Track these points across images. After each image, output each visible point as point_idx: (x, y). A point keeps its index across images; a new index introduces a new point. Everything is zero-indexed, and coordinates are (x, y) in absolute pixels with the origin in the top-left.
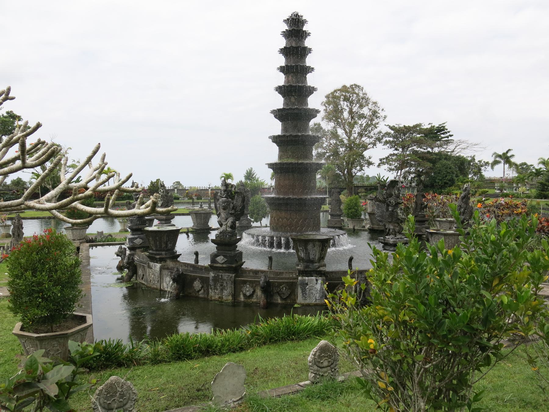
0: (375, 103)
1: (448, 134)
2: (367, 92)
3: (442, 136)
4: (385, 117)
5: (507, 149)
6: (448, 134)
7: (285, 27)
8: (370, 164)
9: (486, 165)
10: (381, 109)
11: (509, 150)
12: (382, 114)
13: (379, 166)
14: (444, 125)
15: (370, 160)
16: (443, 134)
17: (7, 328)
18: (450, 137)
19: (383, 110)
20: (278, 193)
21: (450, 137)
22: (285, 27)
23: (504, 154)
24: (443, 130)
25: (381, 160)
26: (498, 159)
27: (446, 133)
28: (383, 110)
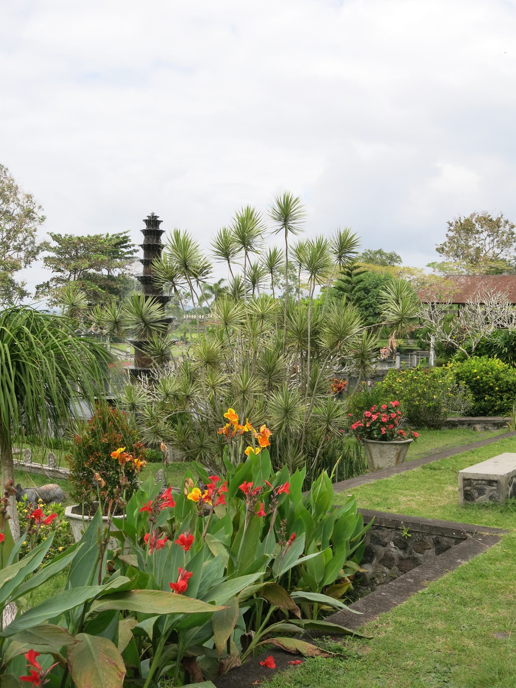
0: (29, 197)
1: (132, 249)
2: (14, 177)
3: (124, 250)
4: (43, 219)
5: (220, 279)
6: (132, 249)
7: (144, 227)
8: (23, 294)
9: (186, 298)
10: (37, 205)
11: (222, 280)
12: (39, 213)
13: (37, 297)
14: (127, 235)
15: (25, 288)
16: (125, 247)
17: (460, 375)
18: (134, 253)
19: (40, 207)
20: (136, 366)
21: (134, 253)
22: (144, 227)
23: (216, 285)
24: (126, 242)
25: (38, 288)
26: (207, 292)
27: (130, 246)
28: (40, 207)
